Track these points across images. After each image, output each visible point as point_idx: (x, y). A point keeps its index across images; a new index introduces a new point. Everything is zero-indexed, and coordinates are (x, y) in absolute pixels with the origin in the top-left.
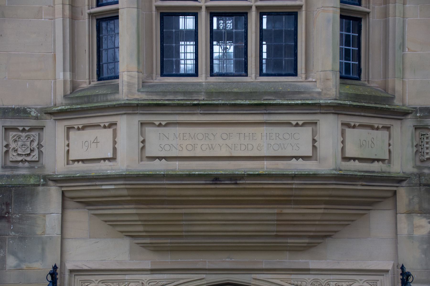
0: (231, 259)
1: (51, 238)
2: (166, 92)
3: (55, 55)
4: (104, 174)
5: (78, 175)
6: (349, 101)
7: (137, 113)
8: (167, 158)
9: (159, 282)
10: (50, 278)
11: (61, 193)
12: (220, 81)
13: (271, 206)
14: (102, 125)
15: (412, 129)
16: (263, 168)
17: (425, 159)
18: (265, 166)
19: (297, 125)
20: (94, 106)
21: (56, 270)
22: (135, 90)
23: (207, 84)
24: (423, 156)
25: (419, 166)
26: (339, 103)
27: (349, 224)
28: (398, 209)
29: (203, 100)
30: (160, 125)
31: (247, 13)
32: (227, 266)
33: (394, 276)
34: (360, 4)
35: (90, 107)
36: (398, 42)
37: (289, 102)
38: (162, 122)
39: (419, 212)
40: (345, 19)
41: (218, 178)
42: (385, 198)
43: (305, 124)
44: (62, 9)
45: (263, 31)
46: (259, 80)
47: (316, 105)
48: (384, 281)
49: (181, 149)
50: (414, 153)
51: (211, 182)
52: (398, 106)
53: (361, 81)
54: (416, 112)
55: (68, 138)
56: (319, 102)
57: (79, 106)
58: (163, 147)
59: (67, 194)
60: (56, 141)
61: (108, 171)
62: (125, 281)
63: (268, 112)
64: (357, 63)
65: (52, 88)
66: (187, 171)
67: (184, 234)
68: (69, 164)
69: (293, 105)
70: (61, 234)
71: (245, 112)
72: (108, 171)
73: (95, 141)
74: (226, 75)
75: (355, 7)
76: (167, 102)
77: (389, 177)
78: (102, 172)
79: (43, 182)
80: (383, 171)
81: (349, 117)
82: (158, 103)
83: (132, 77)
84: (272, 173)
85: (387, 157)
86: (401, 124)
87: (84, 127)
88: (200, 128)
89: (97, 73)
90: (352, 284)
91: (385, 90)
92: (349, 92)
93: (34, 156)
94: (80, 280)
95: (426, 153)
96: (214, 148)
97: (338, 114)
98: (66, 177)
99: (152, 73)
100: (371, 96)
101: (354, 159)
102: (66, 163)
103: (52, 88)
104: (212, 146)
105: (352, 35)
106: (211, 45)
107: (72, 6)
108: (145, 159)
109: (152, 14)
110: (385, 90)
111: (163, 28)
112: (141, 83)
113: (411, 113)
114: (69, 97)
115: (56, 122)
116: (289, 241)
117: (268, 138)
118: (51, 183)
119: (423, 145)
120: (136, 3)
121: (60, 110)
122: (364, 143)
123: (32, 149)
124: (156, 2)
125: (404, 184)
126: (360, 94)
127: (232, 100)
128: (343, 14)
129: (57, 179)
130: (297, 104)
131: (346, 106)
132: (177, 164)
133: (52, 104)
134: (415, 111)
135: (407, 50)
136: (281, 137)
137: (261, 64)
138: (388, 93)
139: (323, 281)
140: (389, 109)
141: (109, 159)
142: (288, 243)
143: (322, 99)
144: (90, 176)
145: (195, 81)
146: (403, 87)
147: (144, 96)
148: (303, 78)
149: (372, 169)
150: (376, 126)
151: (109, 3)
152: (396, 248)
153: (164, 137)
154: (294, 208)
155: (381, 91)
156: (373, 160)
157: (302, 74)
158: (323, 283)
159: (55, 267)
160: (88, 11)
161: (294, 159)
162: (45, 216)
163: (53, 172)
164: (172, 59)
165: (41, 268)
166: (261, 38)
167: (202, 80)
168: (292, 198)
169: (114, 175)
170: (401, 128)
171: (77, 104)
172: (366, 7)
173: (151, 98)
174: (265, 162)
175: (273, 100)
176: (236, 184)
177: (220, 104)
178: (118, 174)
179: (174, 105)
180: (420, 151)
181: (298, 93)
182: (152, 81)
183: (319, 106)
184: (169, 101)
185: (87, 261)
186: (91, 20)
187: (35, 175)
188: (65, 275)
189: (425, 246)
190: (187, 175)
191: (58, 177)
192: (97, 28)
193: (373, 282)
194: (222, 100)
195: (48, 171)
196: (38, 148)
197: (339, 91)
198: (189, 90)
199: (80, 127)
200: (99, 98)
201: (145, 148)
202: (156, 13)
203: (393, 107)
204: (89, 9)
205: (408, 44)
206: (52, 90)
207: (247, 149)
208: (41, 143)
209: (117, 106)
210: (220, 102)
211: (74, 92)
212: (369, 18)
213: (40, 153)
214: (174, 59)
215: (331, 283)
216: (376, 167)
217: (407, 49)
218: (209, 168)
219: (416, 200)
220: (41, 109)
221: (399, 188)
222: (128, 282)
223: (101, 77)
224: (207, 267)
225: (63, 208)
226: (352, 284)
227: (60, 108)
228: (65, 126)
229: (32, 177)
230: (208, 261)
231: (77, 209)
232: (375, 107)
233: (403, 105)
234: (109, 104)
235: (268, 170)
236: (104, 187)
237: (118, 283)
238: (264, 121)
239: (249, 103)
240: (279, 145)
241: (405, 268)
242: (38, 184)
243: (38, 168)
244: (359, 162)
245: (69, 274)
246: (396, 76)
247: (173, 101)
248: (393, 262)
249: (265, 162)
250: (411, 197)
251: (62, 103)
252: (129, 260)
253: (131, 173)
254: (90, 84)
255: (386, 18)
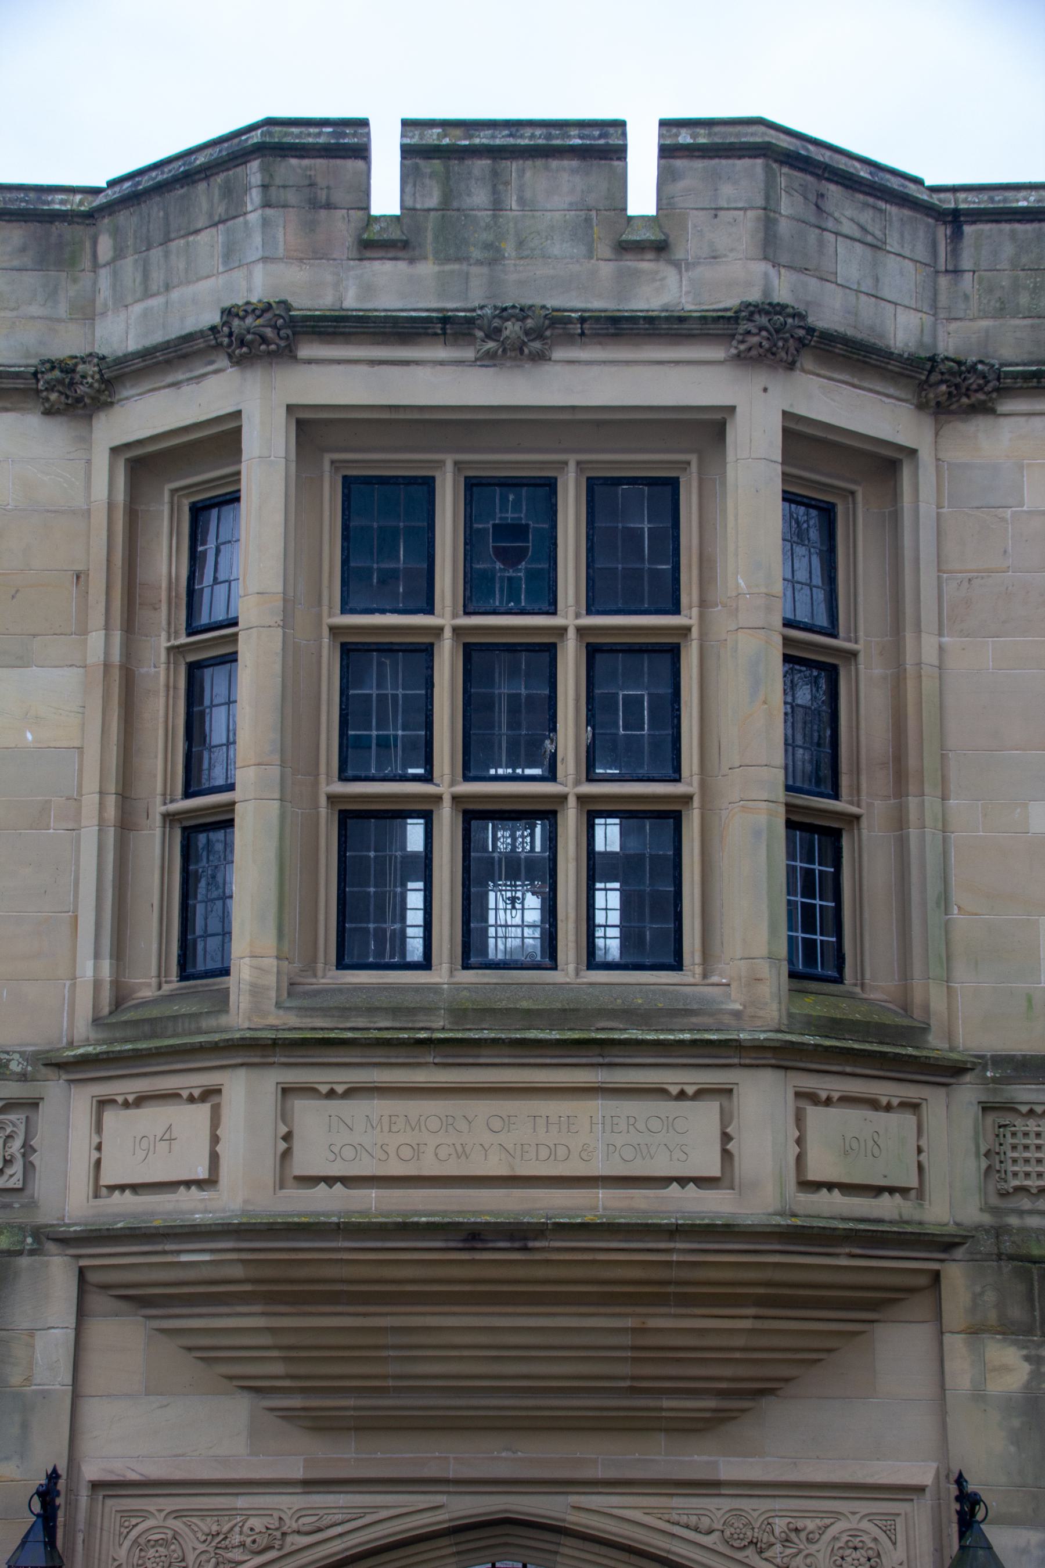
0: (514, 1453)
1: (45, 1394)
2: (349, 1009)
3: (75, 920)
4: (186, 1223)
5: (120, 1225)
6: (812, 1036)
7: (274, 1063)
8: (346, 1181)
9: (326, 1516)
10: (37, 1507)
11: (77, 1273)
12: (486, 980)
13: (618, 1310)
14: (185, 1094)
15: (977, 1110)
16: (596, 1208)
17: (1011, 1190)
18: (600, 1203)
19: (682, 1095)
20: (166, 1046)
21: (56, 1484)
22: (270, 1003)
23: (455, 988)
24: (1006, 1182)
25: (996, 1208)
26: (787, 1041)
27: (820, 1360)
28: (944, 1321)
29: (443, 1029)
30: (331, 1094)
31: (554, 813)
32: (503, 1471)
33: (940, 1504)
34: (836, 796)
35: (156, 1048)
36: (933, 890)
37: (662, 1037)
38: (336, 1087)
39: (998, 1329)
40: (801, 830)
41: (479, 1234)
42: (911, 1290)
43: (701, 1094)
44: (98, 806)
45: (596, 856)
46: (585, 980)
47: (730, 1044)
48: (914, 1516)
49: (384, 1157)
50: (983, 1171)
51: (460, 1245)
52: (937, 1050)
53: (844, 984)
54: (985, 1068)
55: (99, 1128)
56: (737, 1037)
57: (129, 1047)
58: (337, 1152)
59: (92, 1277)
60: (68, 1137)
61: (197, 1216)
62: (234, 1512)
63: (607, 1060)
64: (834, 939)
65: (66, 1002)
66: (398, 1215)
67: (391, 1383)
68: (100, 1197)
69: (671, 1045)
70: (73, 1385)
71: (548, 1061)
72: (197, 1216)
73: (167, 1137)
74: (502, 966)
75: (824, 803)
76: (350, 1035)
77: (920, 1234)
78: (181, 1217)
79: (32, 1244)
80: (906, 1217)
81: (815, 1076)
82: (326, 1036)
83: (264, 970)
84: (617, 1221)
85: (914, 1183)
86: (948, 1095)
87: (141, 1101)
88: (432, 1103)
89: (179, 961)
90: (832, 1524)
91: (906, 1010)
92: (814, 1014)
93: (11, 1176)
94: (116, 1511)
95: (1011, 1174)
96: (468, 1153)
97: (786, 1068)
98: (91, 1230)
99: (314, 960)
100: (869, 1022)
101: (830, 1186)
102: (91, 1194)
103: (66, 1002)
104: (463, 1148)
105: (819, 870)
106: (466, 890)
107: (123, 797)
108: (290, 1182)
109: (318, 814)
110: (906, 1010)
111: (346, 848)
112: (285, 985)
113: (972, 1069)
114: (106, 1022)
115: (72, 1087)
116: (666, 1403)
117: (608, 1128)
118: (51, 1247)
119: (1005, 1153)
120: (277, 789)
121: (82, 1055)
122: (855, 1145)
123: (8, 1158)
124: (328, 784)
125: (959, 1253)
126: (841, 1019)
127: (515, 1030)
128: (795, 818)
129: (68, 1236)
130: (681, 1042)
131: (805, 1047)
132: (374, 1195)
133: (65, 1040)
134: (980, 1063)
135: (956, 911)
136: (641, 1126)
137: (591, 938)
138: (912, 1017)
139: (755, 1514)
140: (916, 1057)
141: (200, 1184)
142: (661, 1409)
143: (744, 1030)
144: (150, 1227)
145: (423, 981)
146: (949, 1004)
147: (293, 1020)
148: (697, 976)
149: (875, 1214)
150: (884, 1101)
151: (214, 787)
152: (944, 1426)
153: (342, 1124)
154: (675, 1316)
155: (895, 1013)
156: (878, 1190)
157: (693, 964)
158: (756, 1520)
159: (53, 1476)
160: (163, 809)
161: (675, 1184)
162: (32, 1336)
163: (58, 1219)
164: (365, 925)
165: (18, 1477)
166: (591, 873)
167: (441, 978)
168: (671, 1289)
169: (210, 1225)
170: (947, 1107)
171: (126, 1041)
172: (851, 803)
173: (310, 1025)
174: (601, 1193)
175: (620, 1030)
176: (525, 1249)
177: (486, 1040)
178: (220, 1221)
179: (368, 1041)
180: (998, 1168)
181: (683, 1012)
182: (314, 980)
183: (736, 1047)
184: (355, 1032)
185: (138, 1457)
186: (168, 829)
187: (13, 1227)
188: (78, 1495)
189: (1016, 1423)
190: (397, 1224)
191: (69, 1231)
192: (182, 851)
193: (886, 1520)
194: (491, 1029)
195: (46, 1216)
196: (24, 1155)
197: (788, 1009)
198: (406, 1004)
199: (131, 1098)
200: (180, 1024)
201: (292, 1153)
202: (328, 813)
203: (925, 1053)
204: (165, 804)
205: (958, 896)
206: (66, 1005)
207: (552, 1157)
208: (32, 1143)
209: (221, 1044)
210: (486, 1034)
211: (119, 1009)
212: (859, 829)
213: (29, 1168)
214: (371, 926)
215: (777, 1520)
216: (886, 1207)
217: (955, 907)
218: (456, 1208)
219: (990, 1297)
220: (36, 1054)
221: (946, 1265)
222: (242, 1515)
223: (190, 970)
224: (451, 1475)
225: (81, 1313)
226: (832, 1524)
227: (81, 1051)
228: (93, 1097)
229: (5, 1231)
230: (455, 1458)
231: (116, 1316)
232: (881, 1052)
233: (952, 1049)
234: (202, 1040)
235: (608, 1213)
236: (184, 1258)
237: (216, 1518)
238: (596, 1085)
239: (558, 1037)
240: (637, 1147)
241: (966, 1482)
242: (19, 1250)
243: (22, 1206)
244: (843, 1195)
245: (90, 1494)
246: (931, 975)
247: (365, 1032)
248: (935, 1465)
249: (601, 1191)
250: (978, 1289)
251: (88, 1039)
252: (248, 1455)
253: (254, 1221)
254: (160, 987)
255: (902, 829)
